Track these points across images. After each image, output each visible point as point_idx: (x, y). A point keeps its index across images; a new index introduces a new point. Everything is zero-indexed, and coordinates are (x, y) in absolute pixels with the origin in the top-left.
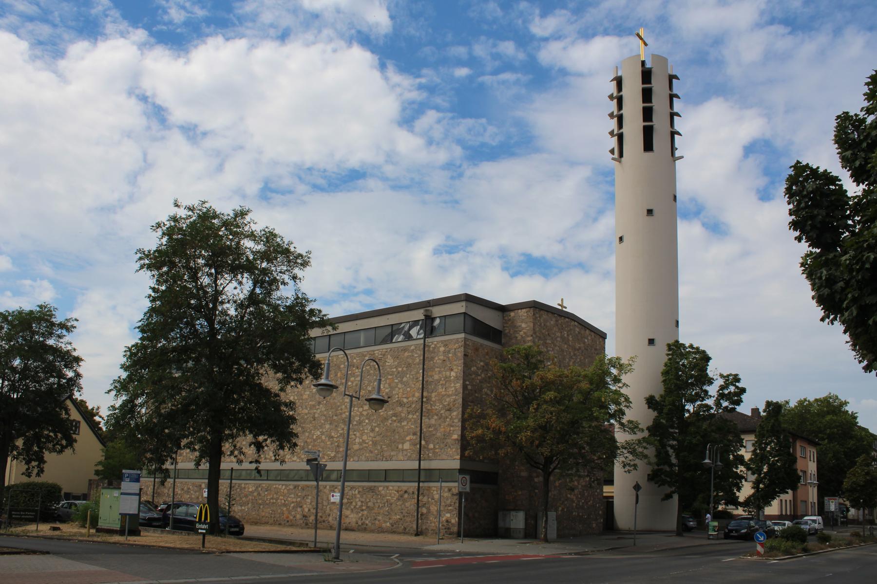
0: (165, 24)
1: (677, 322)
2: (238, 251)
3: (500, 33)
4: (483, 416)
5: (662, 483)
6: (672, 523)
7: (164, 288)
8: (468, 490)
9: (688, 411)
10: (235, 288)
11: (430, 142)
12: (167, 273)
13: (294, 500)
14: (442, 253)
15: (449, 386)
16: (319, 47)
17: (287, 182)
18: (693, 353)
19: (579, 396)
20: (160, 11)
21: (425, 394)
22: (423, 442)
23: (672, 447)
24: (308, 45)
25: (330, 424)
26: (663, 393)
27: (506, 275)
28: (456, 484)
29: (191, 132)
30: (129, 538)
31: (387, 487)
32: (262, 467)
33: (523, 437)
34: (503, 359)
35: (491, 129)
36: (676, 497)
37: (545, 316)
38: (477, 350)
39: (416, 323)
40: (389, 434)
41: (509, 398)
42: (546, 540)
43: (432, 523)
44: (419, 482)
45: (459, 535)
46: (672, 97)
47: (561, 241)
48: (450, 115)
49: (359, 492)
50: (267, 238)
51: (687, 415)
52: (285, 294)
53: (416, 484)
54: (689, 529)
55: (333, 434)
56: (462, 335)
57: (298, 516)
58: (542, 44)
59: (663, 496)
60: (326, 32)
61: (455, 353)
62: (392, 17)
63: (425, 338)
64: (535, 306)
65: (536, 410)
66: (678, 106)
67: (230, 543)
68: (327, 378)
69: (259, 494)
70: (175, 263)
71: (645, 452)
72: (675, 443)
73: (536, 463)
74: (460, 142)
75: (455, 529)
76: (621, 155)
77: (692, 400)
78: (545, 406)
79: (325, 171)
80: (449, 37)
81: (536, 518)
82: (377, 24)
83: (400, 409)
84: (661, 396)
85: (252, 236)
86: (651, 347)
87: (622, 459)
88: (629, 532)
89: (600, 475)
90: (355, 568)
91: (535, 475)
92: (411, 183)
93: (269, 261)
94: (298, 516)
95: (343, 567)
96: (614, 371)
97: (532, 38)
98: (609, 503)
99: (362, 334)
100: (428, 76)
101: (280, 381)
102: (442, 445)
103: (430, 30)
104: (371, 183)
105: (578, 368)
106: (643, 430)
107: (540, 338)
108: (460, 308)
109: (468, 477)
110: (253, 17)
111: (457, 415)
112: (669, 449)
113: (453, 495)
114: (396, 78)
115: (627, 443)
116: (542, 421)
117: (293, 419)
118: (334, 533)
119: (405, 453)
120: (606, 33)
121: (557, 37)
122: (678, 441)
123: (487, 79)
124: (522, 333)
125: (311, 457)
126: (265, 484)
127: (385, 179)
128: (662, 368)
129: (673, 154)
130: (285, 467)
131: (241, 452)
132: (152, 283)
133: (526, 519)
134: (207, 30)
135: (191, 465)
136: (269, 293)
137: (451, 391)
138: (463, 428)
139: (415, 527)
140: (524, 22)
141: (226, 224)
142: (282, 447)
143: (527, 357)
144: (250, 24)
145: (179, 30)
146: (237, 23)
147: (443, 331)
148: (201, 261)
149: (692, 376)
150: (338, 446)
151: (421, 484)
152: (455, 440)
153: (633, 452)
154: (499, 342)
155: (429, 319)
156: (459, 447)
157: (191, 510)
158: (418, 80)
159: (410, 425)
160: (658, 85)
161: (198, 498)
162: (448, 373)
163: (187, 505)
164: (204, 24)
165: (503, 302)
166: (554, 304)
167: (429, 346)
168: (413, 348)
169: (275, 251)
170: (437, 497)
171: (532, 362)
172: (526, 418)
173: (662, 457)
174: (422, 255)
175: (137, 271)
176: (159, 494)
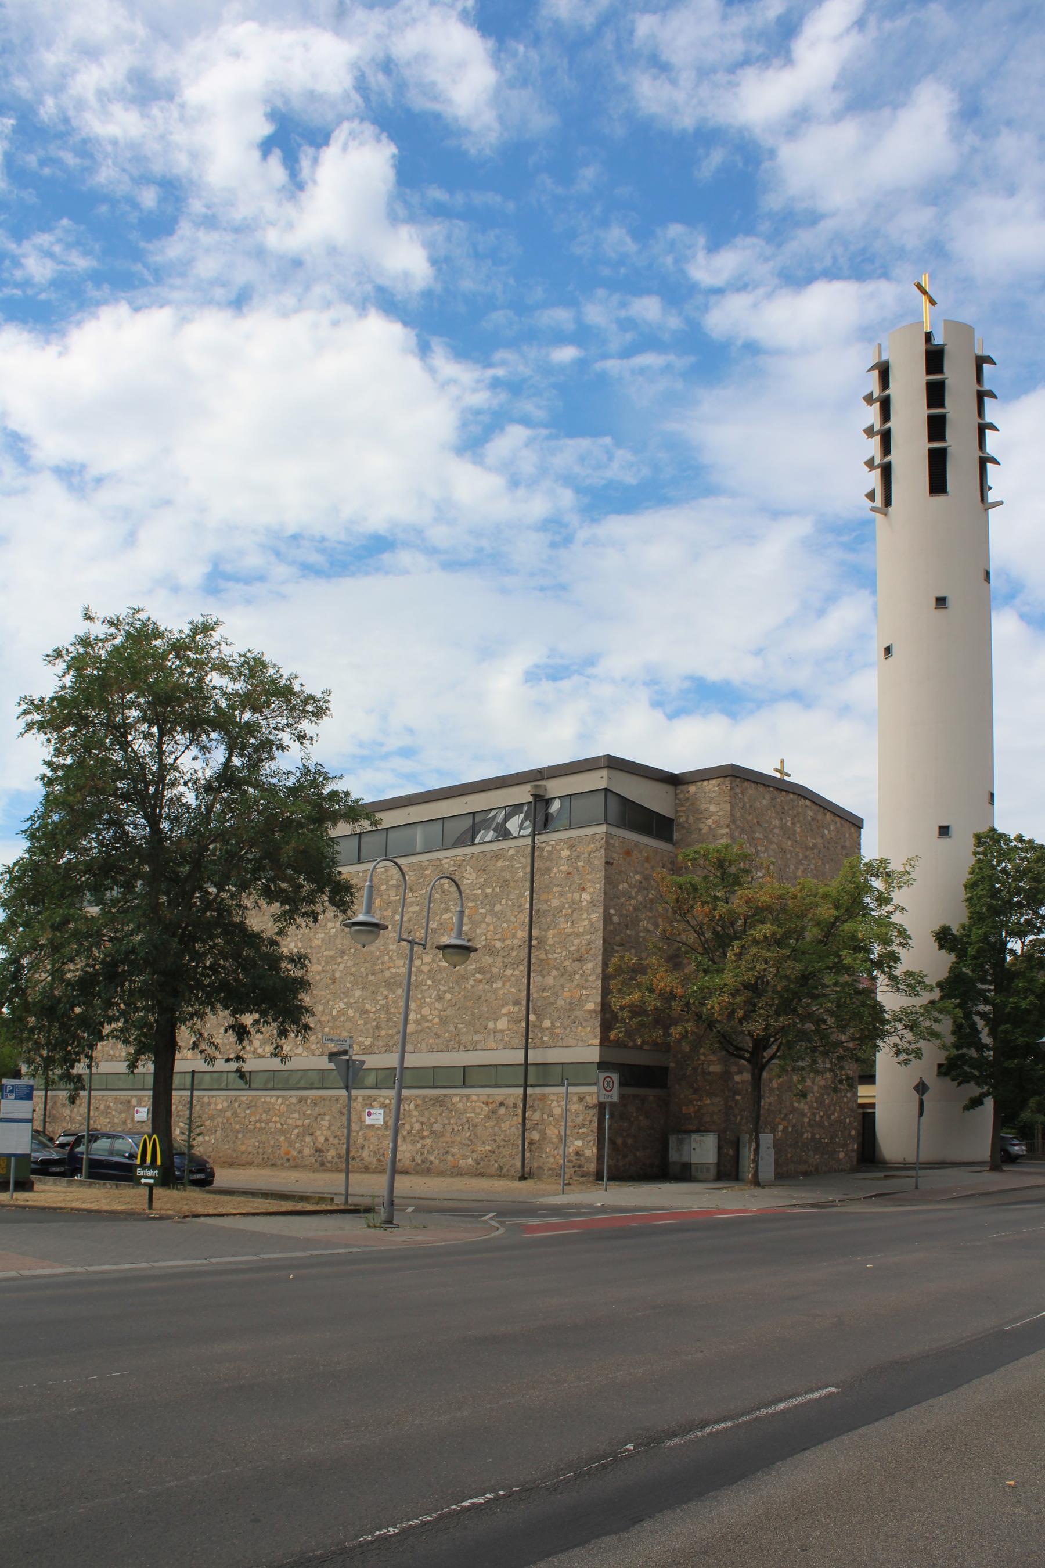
0: (17, 285)
1: (992, 795)
2: (199, 693)
3: (634, 283)
4: (640, 969)
5: (966, 1079)
6: (983, 1149)
7: (69, 761)
8: (615, 1098)
9: (1013, 952)
10: (195, 758)
11: (514, 483)
12: (73, 735)
13: (299, 1123)
14: (540, 680)
15: (579, 917)
16: (309, 317)
17: (254, 561)
18: (1022, 849)
19: (816, 930)
20: (7, 263)
21: (535, 933)
22: (532, 1017)
23: (983, 1015)
24: (285, 314)
25: (363, 989)
26: (966, 921)
27: (659, 715)
28: (594, 1089)
29: (73, 476)
30: (16, 1195)
31: (468, 1097)
32: (247, 1067)
33: (715, 1004)
34: (676, 869)
35: (623, 455)
36: (989, 1103)
37: (751, 790)
38: (628, 853)
39: (517, 808)
40: (470, 1004)
41: (691, 937)
42: (756, 1183)
43: (551, 1157)
44: (526, 1086)
45: (599, 1176)
46: (981, 396)
47: (758, 652)
48: (544, 432)
49: (416, 1106)
50: (251, 669)
51: (1009, 958)
52: (286, 764)
53: (521, 1090)
54: (1012, 1159)
55: (368, 1007)
56: (603, 829)
57: (307, 1151)
58: (713, 299)
59: (966, 1102)
60: (319, 290)
61: (589, 861)
62: (434, 262)
63: (534, 835)
64: (736, 776)
65: (739, 956)
66: (992, 412)
67: (191, 1198)
68: (369, 911)
69: (235, 1114)
70: (87, 717)
71: (936, 1027)
72: (988, 1008)
73: (738, 1049)
74: (568, 480)
75: (592, 1167)
76: (888, 501)
77: (1021, 934)
78: (754, 950)
79: (323, 539)
80: (539, 293)
81: (737, 1145)
82: (407, 275)
83: (489, 960)
84: (963, 927)
85: (222, 668)
86: (944, 841)
87: (893, 1039)
88: (905, 1166)
89: (852, 1069)
90: (422, 1238)
91: (734, 1069)
92: (480, 557)
93: (255, 709)
94: (307, 1151)
95: (402, 1237)
96: (877, 883)
97: (693, 288)
98: (867, 1117)
99: (419, 831)
100: (508, 363)
101: (277, 918)
102: (567, 1022)
103: (512, 281)
104: (405, 558)
105: (810, 881)
106: (932, 990)
107: (743, 830)
108: (598, 780)
109: (615, 1077)
110: (183, 268)
111: (593, 969)
112: (977, 1018)
113: (587, 1107)
114: (449, 368)
115: (904, 1011)
116: (750, 976)
117: (303, 984)
118: (383, 1180)
119: (499, 1036)
120: (831, 274)
121: (740, 285)
122: (994, 1005)
123: (612, 365)
124: (709, 822)
125: (333, 1047)
126: (246, 1095)
127: (432, 551)
128: (965, 877)
129: (983, 497)
130: (289, 1065)
131: (207, 1041)
132: (47, 752)
133: (720, 1148)
134: (96, 294)
135: (122, 1067)
136: (254, 766)
137: (582, 926)
138: (605, 992)
139: (519, 1164)
140: (676, 261)
141: (178, 648)
142: (283, 1033)
143: (721, 864)
144: (178, 282)
145: (43, 296)
146: (151, 279)
147: (566, 822)
148: (134, 714)
149: (1019, 891)
150: (377, 1027)
151: (529, 1090)
152: (590, 1011)
153: (912, 1027)
154: (669, 839)
155: (541, 801)
156: (598, 1024)
157: (119, 1145)
158: (490, 372)
159: (508, 987)
160: (957, 376)
161: (125, 1123)
162: (576, 896)
163: (109, 1136)
164: (90, 284)
165: (676, 767)
166: (766, 767)
167: (542, 849)
168: (511, 852)
169: (268, 693)
170: (557, 1111)
171: (728, 872)
172: (720, 971)
173: (965, 1034)
174: (504, 683)
175: (22, 734)
176: (54, 1119)
